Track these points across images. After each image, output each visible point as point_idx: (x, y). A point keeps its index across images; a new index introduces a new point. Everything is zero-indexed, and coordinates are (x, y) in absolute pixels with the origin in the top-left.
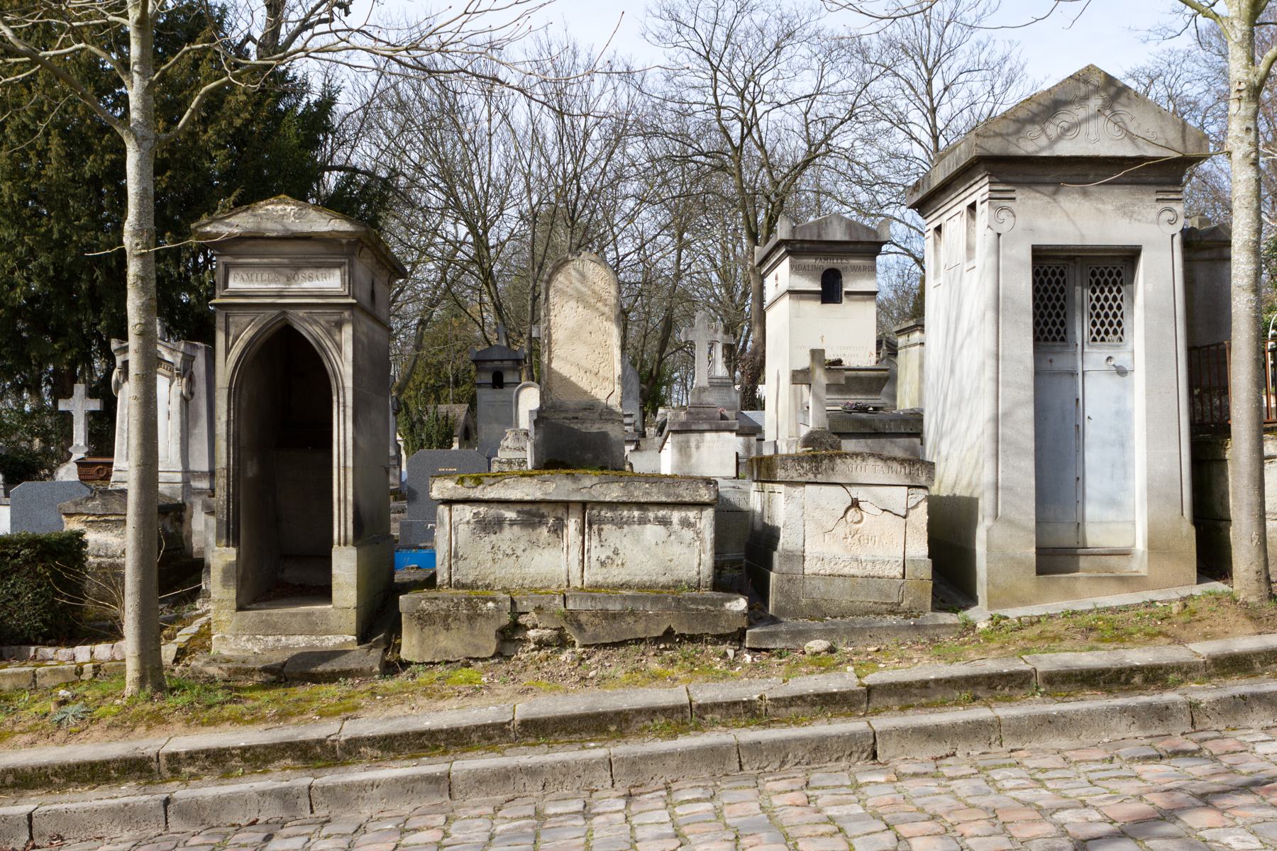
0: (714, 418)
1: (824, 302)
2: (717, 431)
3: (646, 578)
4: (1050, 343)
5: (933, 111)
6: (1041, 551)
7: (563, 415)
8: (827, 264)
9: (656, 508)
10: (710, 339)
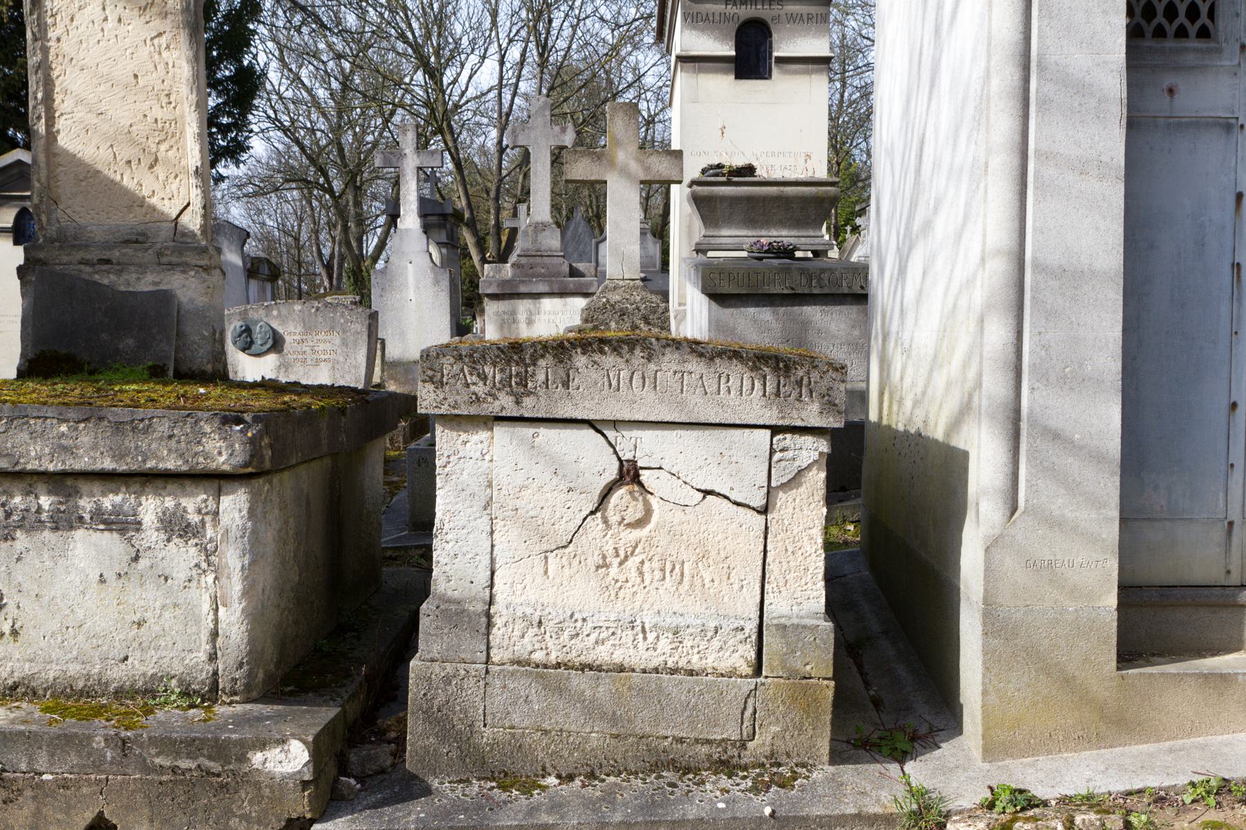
0: (558, 274)
1: (739, 76)
3: (74, 669)
4: (1170, 43)
6: (1131, 593)
7: (80, 255)
8: (746, 12)
9: (96, 487)
10: (554, 142)
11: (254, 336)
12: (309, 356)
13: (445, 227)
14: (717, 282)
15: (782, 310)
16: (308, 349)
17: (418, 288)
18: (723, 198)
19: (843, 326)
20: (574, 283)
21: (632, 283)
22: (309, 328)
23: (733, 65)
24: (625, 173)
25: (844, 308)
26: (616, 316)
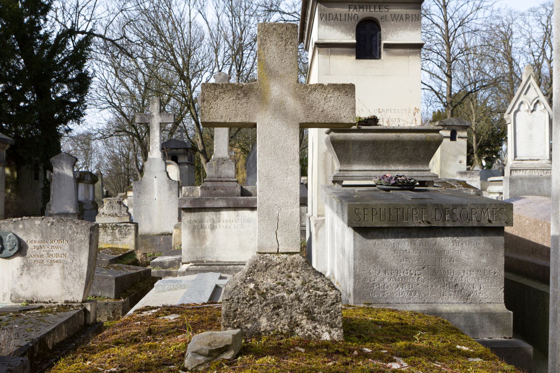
0: (233, 194)
1: (359, 57)
2: (236, 208)
5: (445, 6)
8: (363, 13)
11: (5, 244)
12: (45, 258)
13: (187, 155)
14: (362, 217)
15: (418, 241)
16: (44, 253)
17: (160, 192)
18: (355, 142)
19: (472, 254)
20: (244, 200)
21: (290, 258)
22: (45, 238)
23: (354, 50)
24: (280, 110)
25: (473, 238)
26: (268, 310)
